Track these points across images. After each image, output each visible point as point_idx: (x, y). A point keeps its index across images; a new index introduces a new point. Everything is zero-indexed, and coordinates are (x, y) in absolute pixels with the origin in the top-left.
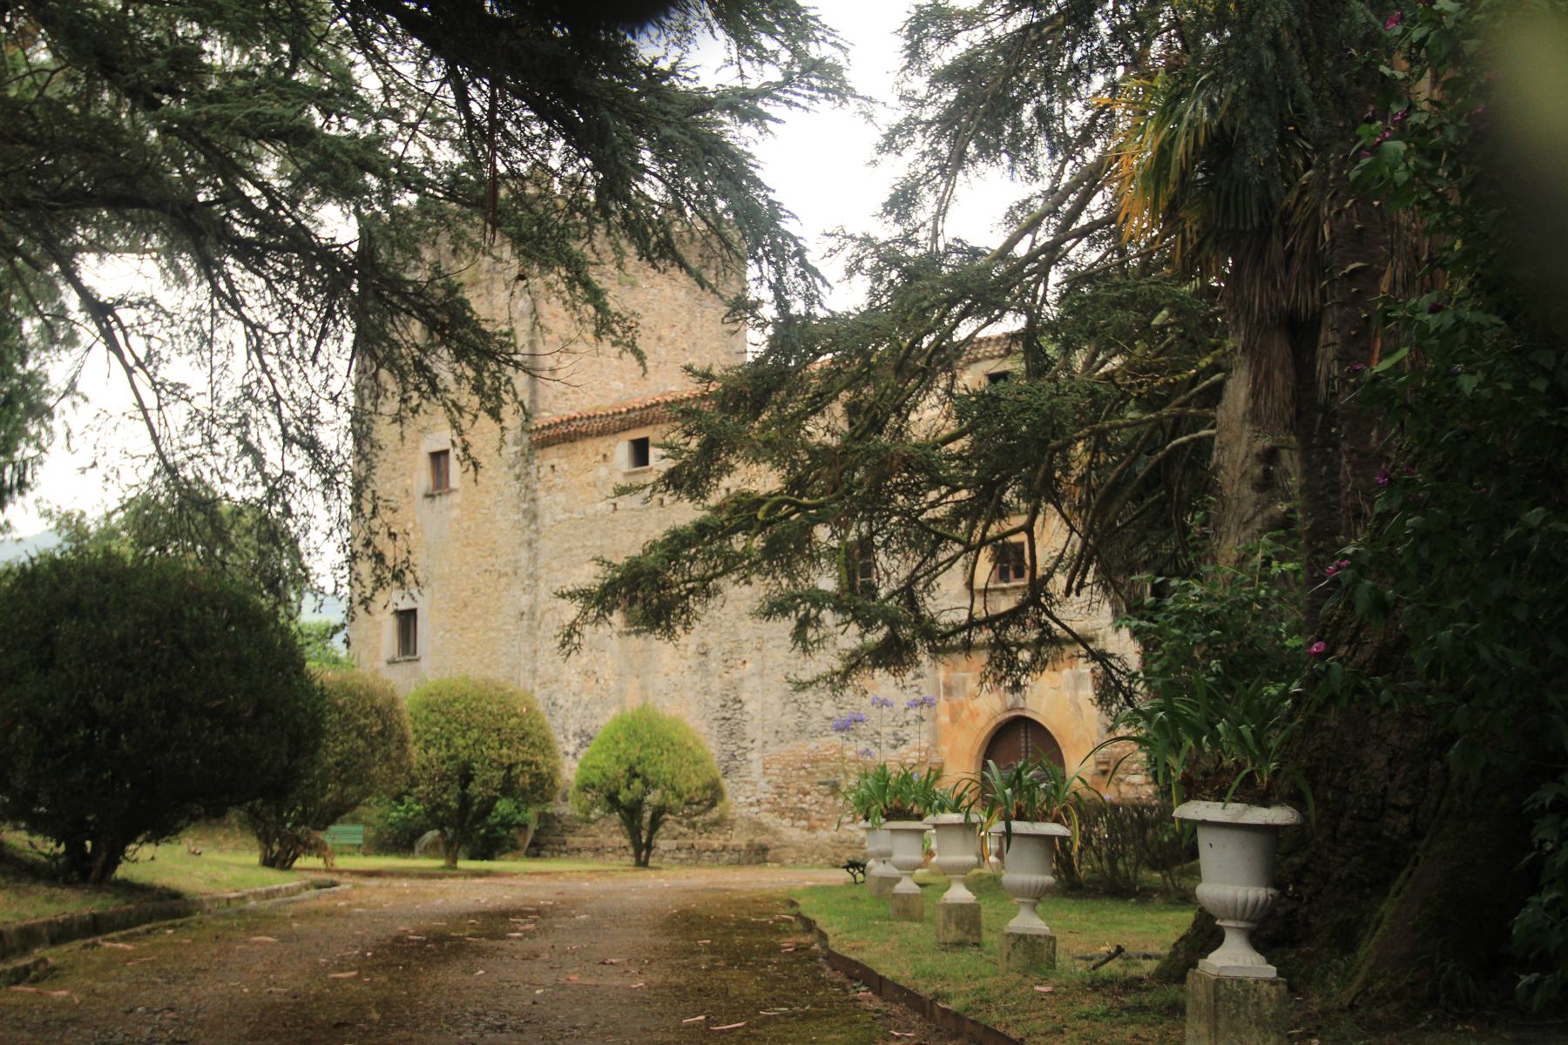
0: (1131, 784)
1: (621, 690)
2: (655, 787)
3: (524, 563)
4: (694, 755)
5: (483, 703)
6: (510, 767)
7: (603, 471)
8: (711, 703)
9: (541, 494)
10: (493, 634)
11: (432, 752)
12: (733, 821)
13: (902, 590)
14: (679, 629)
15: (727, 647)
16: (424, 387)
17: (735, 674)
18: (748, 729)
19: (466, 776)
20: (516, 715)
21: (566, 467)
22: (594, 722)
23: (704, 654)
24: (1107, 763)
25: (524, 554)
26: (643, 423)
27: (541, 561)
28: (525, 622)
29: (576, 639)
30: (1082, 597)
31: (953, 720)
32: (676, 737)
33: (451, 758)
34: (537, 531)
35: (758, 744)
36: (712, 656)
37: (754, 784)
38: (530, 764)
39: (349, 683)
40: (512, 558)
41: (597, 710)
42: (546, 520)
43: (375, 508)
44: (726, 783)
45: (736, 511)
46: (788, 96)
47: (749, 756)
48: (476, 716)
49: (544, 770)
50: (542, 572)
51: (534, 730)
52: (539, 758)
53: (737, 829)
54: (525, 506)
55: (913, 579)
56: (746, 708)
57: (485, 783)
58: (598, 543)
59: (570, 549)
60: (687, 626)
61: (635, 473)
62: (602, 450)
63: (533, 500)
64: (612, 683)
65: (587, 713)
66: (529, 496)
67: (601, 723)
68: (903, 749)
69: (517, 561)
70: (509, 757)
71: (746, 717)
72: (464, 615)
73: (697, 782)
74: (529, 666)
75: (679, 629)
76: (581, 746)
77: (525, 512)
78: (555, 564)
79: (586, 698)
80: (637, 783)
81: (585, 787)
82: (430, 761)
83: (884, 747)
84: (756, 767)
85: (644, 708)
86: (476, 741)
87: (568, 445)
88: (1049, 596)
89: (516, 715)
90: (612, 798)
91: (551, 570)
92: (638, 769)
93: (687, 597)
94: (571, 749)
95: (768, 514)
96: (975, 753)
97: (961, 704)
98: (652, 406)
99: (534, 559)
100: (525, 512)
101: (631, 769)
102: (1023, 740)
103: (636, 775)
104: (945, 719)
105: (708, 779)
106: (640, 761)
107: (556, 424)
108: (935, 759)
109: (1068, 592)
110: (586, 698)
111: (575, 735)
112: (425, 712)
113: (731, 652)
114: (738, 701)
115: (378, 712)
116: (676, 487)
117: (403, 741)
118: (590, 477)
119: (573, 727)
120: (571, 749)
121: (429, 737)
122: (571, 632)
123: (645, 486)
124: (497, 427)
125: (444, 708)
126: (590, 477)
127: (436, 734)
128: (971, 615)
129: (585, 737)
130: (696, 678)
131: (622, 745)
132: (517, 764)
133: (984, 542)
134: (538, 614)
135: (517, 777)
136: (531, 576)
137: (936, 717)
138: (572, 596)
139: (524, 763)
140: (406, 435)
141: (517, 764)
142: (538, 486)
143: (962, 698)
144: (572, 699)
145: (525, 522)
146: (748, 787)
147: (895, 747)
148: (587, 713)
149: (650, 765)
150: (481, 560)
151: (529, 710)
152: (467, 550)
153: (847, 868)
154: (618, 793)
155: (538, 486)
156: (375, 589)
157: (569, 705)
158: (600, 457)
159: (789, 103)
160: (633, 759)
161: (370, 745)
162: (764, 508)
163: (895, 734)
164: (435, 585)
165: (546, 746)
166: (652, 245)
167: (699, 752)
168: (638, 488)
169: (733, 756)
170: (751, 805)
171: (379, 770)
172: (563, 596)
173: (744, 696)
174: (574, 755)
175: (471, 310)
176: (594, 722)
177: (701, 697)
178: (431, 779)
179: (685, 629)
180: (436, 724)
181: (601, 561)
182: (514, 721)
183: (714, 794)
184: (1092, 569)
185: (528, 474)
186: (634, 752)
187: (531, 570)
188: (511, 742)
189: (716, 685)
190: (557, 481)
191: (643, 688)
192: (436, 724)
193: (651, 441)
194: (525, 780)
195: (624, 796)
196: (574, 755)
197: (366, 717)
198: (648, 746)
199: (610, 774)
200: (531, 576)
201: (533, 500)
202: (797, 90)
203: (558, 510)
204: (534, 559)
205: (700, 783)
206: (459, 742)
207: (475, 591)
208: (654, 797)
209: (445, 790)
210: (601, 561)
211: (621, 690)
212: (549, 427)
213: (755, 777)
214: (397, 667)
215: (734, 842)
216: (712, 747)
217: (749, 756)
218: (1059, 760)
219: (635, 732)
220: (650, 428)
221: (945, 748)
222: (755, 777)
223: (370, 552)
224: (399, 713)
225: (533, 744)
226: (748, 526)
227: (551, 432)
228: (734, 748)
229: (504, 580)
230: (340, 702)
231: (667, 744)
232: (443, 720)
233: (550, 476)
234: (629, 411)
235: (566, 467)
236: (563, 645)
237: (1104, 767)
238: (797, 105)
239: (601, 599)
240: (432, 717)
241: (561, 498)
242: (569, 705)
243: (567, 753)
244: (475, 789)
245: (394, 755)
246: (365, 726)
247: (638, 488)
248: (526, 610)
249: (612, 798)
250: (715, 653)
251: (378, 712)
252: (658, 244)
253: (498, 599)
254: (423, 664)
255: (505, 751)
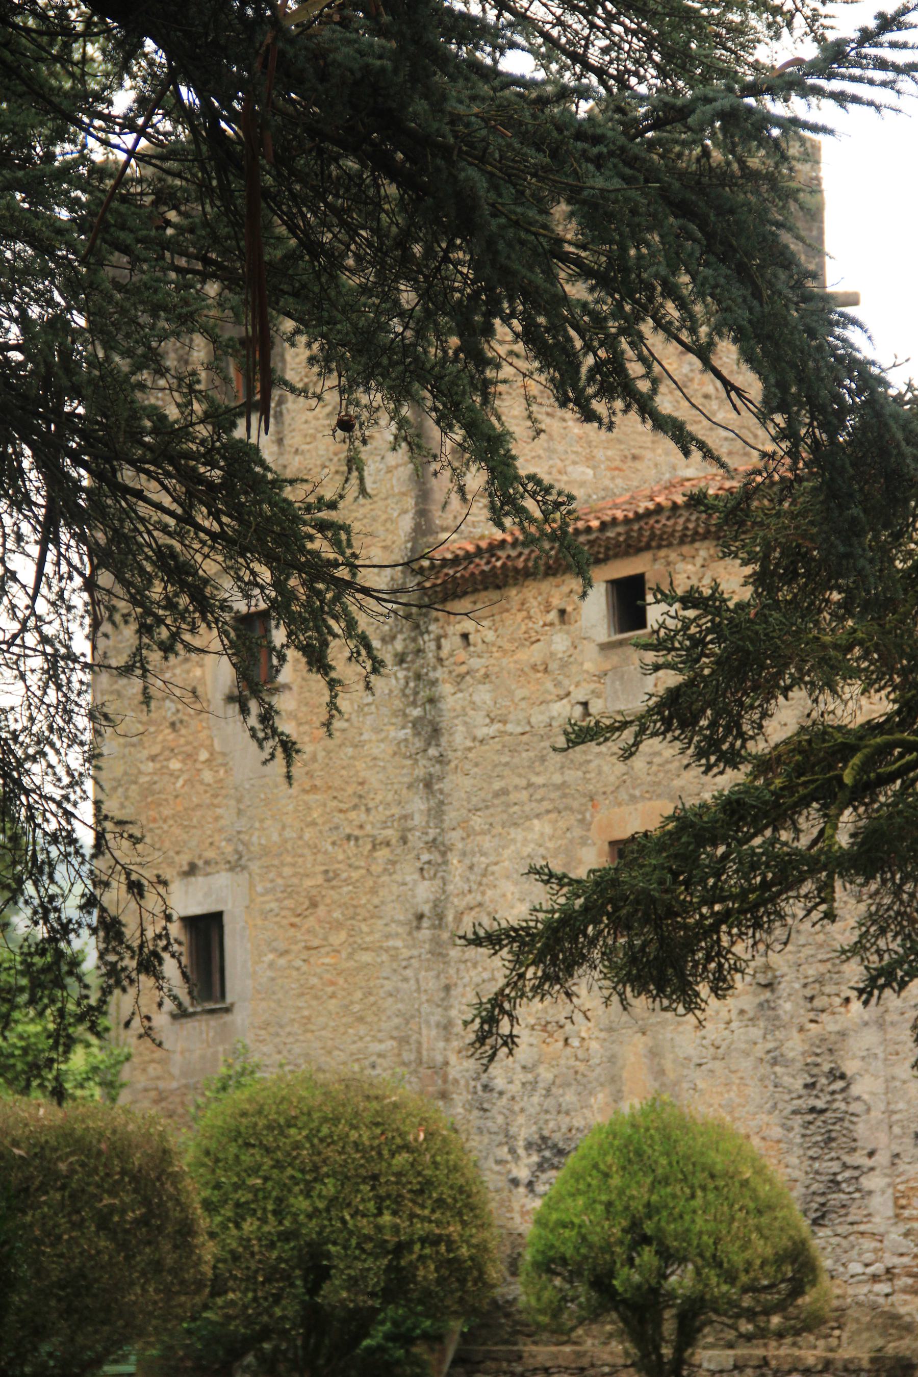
1: (612, 1059)
2: (683, 1260)
3: (418, 820)
4: (755, 1198)
5: (342, 1127)
6: (401, 1248)
7: (560, 642)
8: (787, 1080)
9: (446, 688)
10: (366, 957)
11: (249, 1226)
12: (842, 1310)
14: (704, 989)
15: (812, 971)
16: (184, 601)
17: (830, 1025)
18: (861, 1129)
19: (317, 1270)
20: (406, 1147)
21: (490, 636)
22: (565, 1121)
23: (769, 986)
25: (418, 805)
26: (631, 547)
27: (452, 815)
28: (425, 933)
29: (505, 1026)
32: (719, 1161)
33: (286, 1236)
34: (441, 760)
35: (882, 1158)
36: (783, 988)
37: (879, 1237)
38: (435, 1241)
39: (79, 1128)
40: (396, 811)
41: (569, 1098)
42: (458, 737)
43: (100, 837)
44: (822, 1242)
45: (800, 770)
46: (835, 85)
47: (867, 1182)
48: (329, 1152)
49: (464, 1251)
50: (454, 837)
51: (441, 1174)
52: (454, 1229)
53: (851, 1327)
54: (416, 712)
56: (855, 1090)
57: (353, 1283)
58: (557, 779)
59: (504, 792)
60: (721, 987)
61: (621, 643)
62: (556, 602)
63: (431, 701)
64: (594, 1045)
65: (550, 1103)
66: (424, 694)
67: (578, 1122)
69: (405, 817)
70: (396, 1229)
71: (855, 1107)
72: (311, 922)
73: (762, 1248)
74: (437, 1016)
75: (704, 989)
76: (541, 1167)
77: (416, 723)
78: (477, 821)
79: (546, 1074)
80: (647, 1256)
81: (549, 1264)
82: (245, 1242)
84: (881, 1206)
85: (654, 1106)
86: (333, 1201)
87: (494, 595)
89: (406, 1147)
90: (601, 1283)
91: (470, 833)
92: (649, 1227)
93: (715, 928)
94: (523, 1173)
95: (864, 767)
98: (648, 513)
99: (437, 812)
100: (416, 723)
101: (635, 1225)
103: (646, 1240)
105: (785, 1242)
106: (651, 1210)
107: (468, 557)
110: (546, 1074)
111: (529, 1146)
112: (233, 1149)
113: (820, 981)
114: (837, 1075)
115: (134, 1178)
116: (683, 726)
117: (186, 1229)
118: (535, 654)
119: (524, 1131)
120: (523, 1173)
121: (243, 1196)
122: (493, 1014)
123: (625, 725)
124: (318, 682)
125: (269, 1140)
126: (535, 654)
127: (255, 1190)
129: (550, 1151)
130: (756, 1033)
131: (616, 1181)
132: (411, 1243)
134: (450, 917)
135: (413, 1266)
136: (433, 844)
138: (491, 941)
139: (423, 1241)
140: (152, 691)
141: (411, 1243)
142: (439, 674)
144: (521, 1076)
145: (419, 744)
146: (868, 1244)
148: (550, 1103)
149: (672, 1219)
150: (338, 818)
151: (430, 1135)
152: (311, 798)
154: (611, 1274)
155: (439, 674)
156: (106, 991)
157: (515, 1088)
158: (553, 616)
159: (840, 98)
160: (638, 1207)
161: (123, 1246)
162: (856, 760)
164: (255, 867)
165: (465, 1203)
166: (584, 370)
167: (764, 1190)
168: (612, 729)
169: (834, 1184)
170: (875, 1278)
171: (142, 1294)
172: (477, 941)
173: (850, 1067)
174: (530, 1185)
175: (262, 463)
176: (565, 1121)
177: (765, 1069)
178: (250, 1278)
179: (715, 990)
180: (254, 1170)
181: (548, 877)
182: (402, 1159)
183: (799, 1267)
185: (419, 651)
186: (640, 1193)
187: (432, 833)
188: (398, 1199)
189: (795, 1046)
190: (475, 663)
191: (654, 1053)
192: (254, 1170)
193: (650, 583)
194: (427, 1273)
195: (626, 1279)
196: (530, 1185)
197: (112, 1193)
198: (665, 1181)
199: (594, 1239)
200: (433, 844)
201: (431, 701)
202: (857, 72)
203: (479, 718)
204: (437, 812)
205: (769, 1252)
206: (302, 1204)
207: (330, 877)
208: (681, 1280)
209: (277, 1299)
210: (548, 877)
211: (612, 1059)
212: (456, 561)
213: (879, 1223)
214: (189, 1025)
215: (846, 1353)
216: (786, 1167)
217: (867, 1182)
219: (639, 1153)
220: (647, 556)
222: (879, 1223)
223: (94, 919)
224: (176, 1178)
225: (440, 1203)
226: (831, 796)
227: (458, 572)
228: (835, 1167)
229: (383, 854)
230: (63, 1167)
231: (701, 1177)
232: (268, 1162)
233: (462, 655)
234: (604, 526)
235: (490, 636)
236: (481, 1039)
238: (856, 99)
239: (550, 950)
240: (246, 1159)
241: (483, 695)
242: (515, 1088)
243: (515, 1182)
244: (336, 1293)
245: (169, 1261)
246: (112, 1209)
247: (612, 729)
248: (426, 909)
249: (601, 1283)
250: (790, 984)
251: (134, 1178)
252: (594, 370)
253: (373, 891)
254: (239, 1018)
255: (387, 1218)
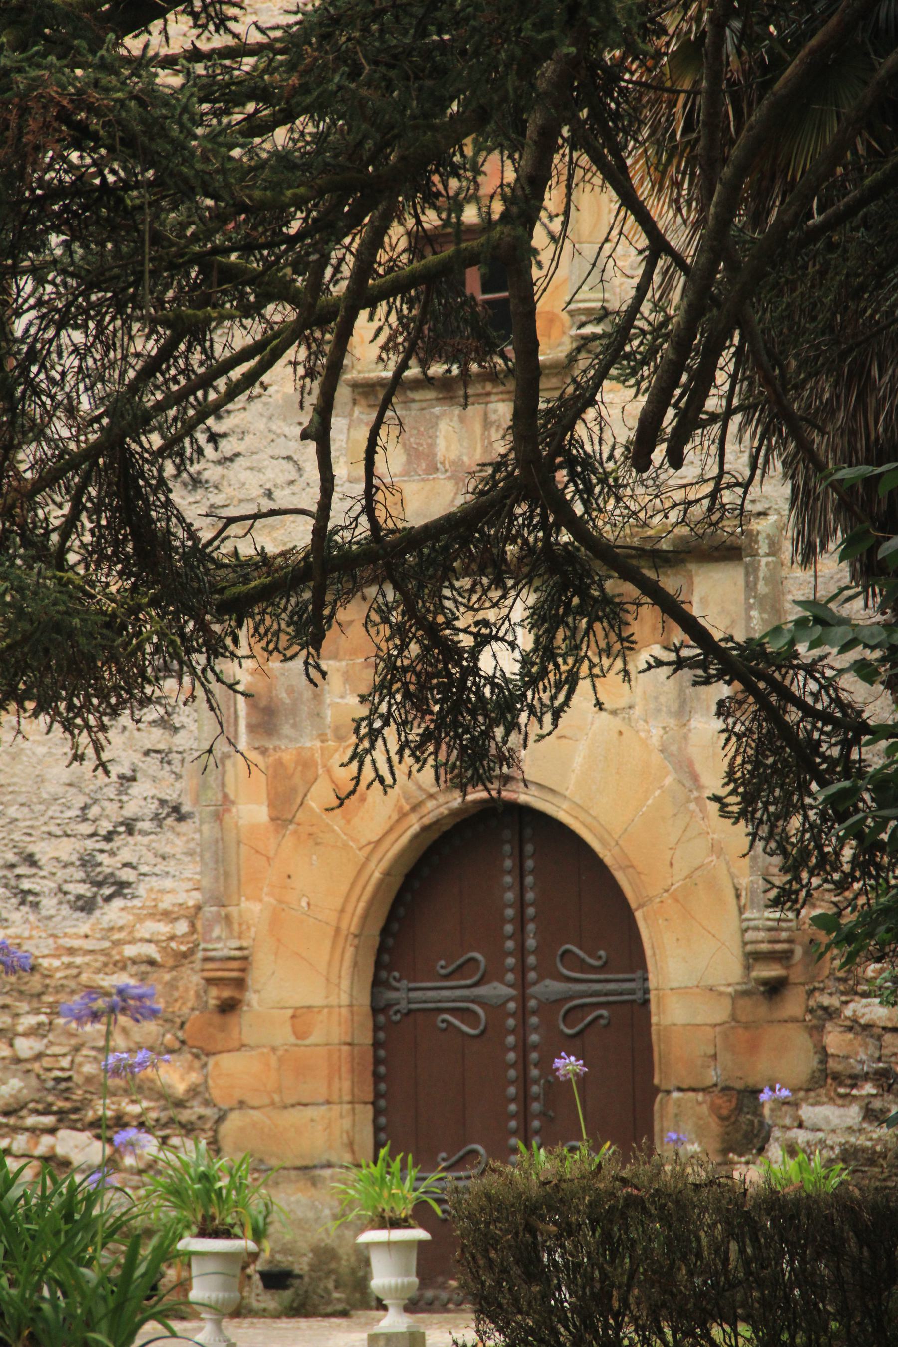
0: (855, 1026)
13: (91, 453)
24: (783, 958)
30: (689, 472)
31: (281, 819)
55: (126, 416)
68: (113, 913)
83: (49, 904)
88: (583, 467)
96: (351, 923)
97: (306, 763)
102: (509, 883)
104: (252, 812)
108: (223, 945)
109: (639, 456)
128: (320, 533)
133: (362, 297)
137: (224, 806)
143: (310, 743)
147: (86, 906)
153: (221, 821)
163: (87, 862)
184: (726, 360)
218: (630, 954)
221: (252, 909)
237: (772, 972)
